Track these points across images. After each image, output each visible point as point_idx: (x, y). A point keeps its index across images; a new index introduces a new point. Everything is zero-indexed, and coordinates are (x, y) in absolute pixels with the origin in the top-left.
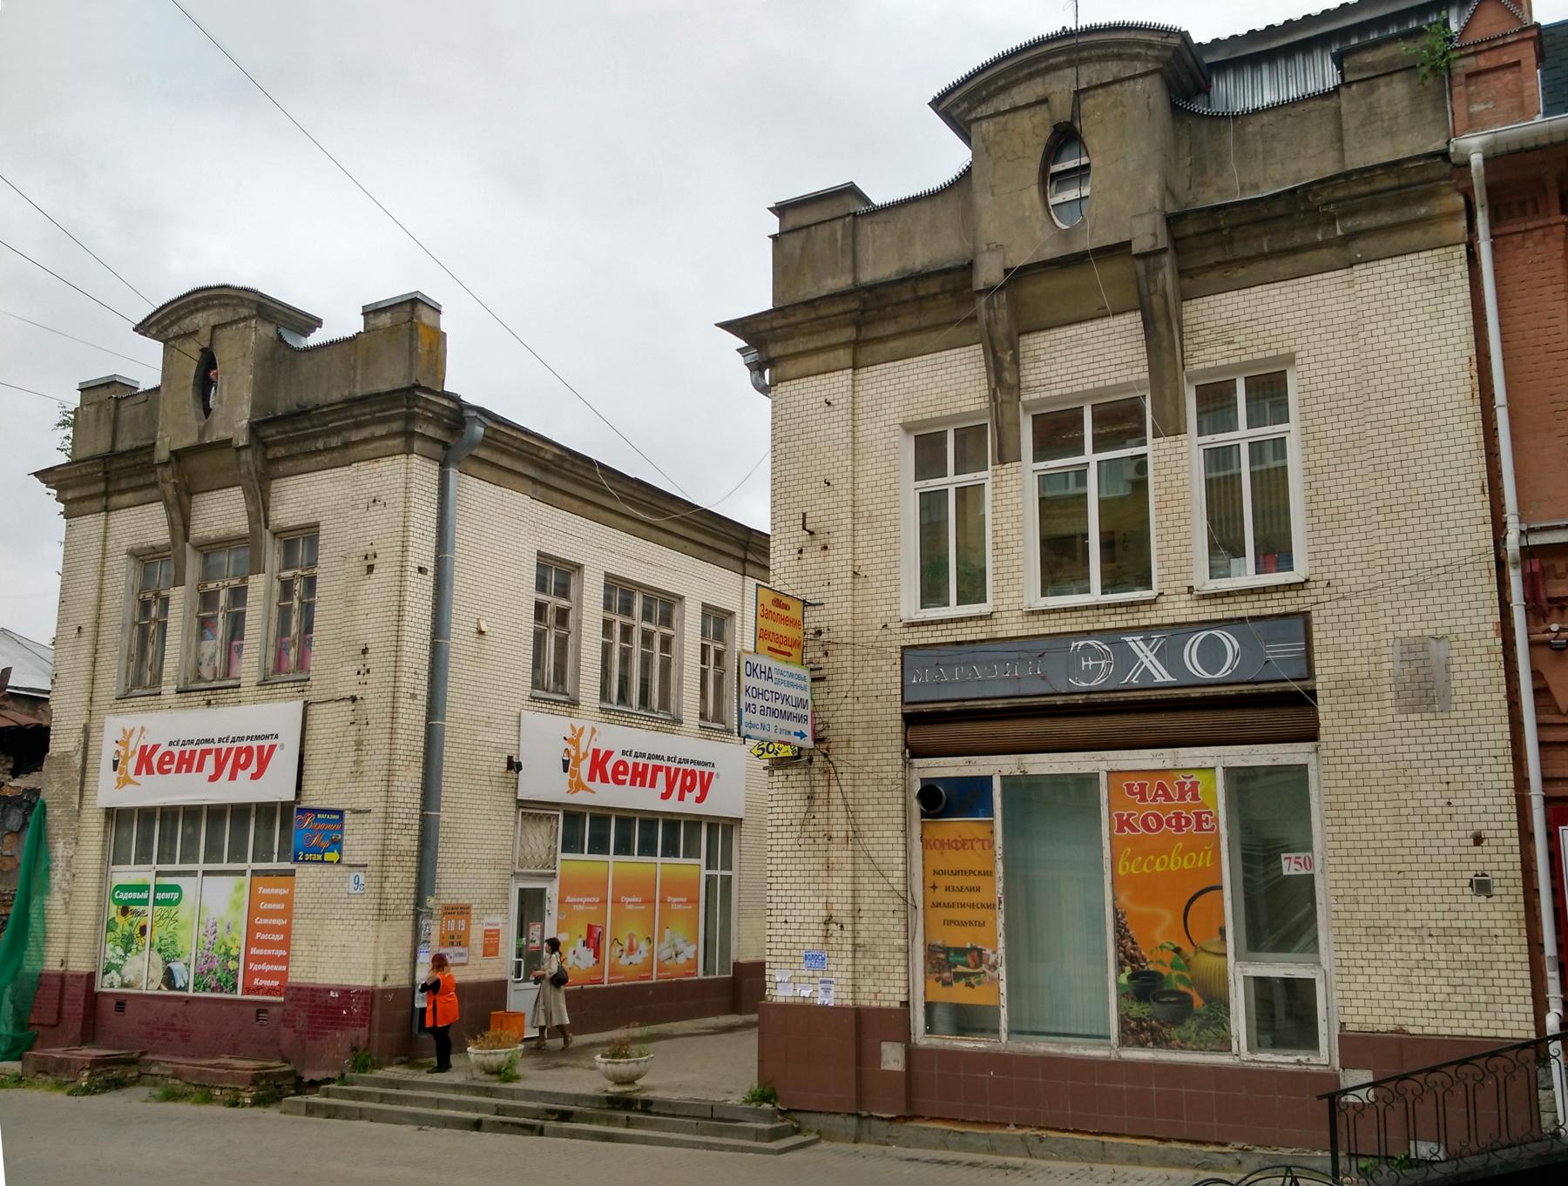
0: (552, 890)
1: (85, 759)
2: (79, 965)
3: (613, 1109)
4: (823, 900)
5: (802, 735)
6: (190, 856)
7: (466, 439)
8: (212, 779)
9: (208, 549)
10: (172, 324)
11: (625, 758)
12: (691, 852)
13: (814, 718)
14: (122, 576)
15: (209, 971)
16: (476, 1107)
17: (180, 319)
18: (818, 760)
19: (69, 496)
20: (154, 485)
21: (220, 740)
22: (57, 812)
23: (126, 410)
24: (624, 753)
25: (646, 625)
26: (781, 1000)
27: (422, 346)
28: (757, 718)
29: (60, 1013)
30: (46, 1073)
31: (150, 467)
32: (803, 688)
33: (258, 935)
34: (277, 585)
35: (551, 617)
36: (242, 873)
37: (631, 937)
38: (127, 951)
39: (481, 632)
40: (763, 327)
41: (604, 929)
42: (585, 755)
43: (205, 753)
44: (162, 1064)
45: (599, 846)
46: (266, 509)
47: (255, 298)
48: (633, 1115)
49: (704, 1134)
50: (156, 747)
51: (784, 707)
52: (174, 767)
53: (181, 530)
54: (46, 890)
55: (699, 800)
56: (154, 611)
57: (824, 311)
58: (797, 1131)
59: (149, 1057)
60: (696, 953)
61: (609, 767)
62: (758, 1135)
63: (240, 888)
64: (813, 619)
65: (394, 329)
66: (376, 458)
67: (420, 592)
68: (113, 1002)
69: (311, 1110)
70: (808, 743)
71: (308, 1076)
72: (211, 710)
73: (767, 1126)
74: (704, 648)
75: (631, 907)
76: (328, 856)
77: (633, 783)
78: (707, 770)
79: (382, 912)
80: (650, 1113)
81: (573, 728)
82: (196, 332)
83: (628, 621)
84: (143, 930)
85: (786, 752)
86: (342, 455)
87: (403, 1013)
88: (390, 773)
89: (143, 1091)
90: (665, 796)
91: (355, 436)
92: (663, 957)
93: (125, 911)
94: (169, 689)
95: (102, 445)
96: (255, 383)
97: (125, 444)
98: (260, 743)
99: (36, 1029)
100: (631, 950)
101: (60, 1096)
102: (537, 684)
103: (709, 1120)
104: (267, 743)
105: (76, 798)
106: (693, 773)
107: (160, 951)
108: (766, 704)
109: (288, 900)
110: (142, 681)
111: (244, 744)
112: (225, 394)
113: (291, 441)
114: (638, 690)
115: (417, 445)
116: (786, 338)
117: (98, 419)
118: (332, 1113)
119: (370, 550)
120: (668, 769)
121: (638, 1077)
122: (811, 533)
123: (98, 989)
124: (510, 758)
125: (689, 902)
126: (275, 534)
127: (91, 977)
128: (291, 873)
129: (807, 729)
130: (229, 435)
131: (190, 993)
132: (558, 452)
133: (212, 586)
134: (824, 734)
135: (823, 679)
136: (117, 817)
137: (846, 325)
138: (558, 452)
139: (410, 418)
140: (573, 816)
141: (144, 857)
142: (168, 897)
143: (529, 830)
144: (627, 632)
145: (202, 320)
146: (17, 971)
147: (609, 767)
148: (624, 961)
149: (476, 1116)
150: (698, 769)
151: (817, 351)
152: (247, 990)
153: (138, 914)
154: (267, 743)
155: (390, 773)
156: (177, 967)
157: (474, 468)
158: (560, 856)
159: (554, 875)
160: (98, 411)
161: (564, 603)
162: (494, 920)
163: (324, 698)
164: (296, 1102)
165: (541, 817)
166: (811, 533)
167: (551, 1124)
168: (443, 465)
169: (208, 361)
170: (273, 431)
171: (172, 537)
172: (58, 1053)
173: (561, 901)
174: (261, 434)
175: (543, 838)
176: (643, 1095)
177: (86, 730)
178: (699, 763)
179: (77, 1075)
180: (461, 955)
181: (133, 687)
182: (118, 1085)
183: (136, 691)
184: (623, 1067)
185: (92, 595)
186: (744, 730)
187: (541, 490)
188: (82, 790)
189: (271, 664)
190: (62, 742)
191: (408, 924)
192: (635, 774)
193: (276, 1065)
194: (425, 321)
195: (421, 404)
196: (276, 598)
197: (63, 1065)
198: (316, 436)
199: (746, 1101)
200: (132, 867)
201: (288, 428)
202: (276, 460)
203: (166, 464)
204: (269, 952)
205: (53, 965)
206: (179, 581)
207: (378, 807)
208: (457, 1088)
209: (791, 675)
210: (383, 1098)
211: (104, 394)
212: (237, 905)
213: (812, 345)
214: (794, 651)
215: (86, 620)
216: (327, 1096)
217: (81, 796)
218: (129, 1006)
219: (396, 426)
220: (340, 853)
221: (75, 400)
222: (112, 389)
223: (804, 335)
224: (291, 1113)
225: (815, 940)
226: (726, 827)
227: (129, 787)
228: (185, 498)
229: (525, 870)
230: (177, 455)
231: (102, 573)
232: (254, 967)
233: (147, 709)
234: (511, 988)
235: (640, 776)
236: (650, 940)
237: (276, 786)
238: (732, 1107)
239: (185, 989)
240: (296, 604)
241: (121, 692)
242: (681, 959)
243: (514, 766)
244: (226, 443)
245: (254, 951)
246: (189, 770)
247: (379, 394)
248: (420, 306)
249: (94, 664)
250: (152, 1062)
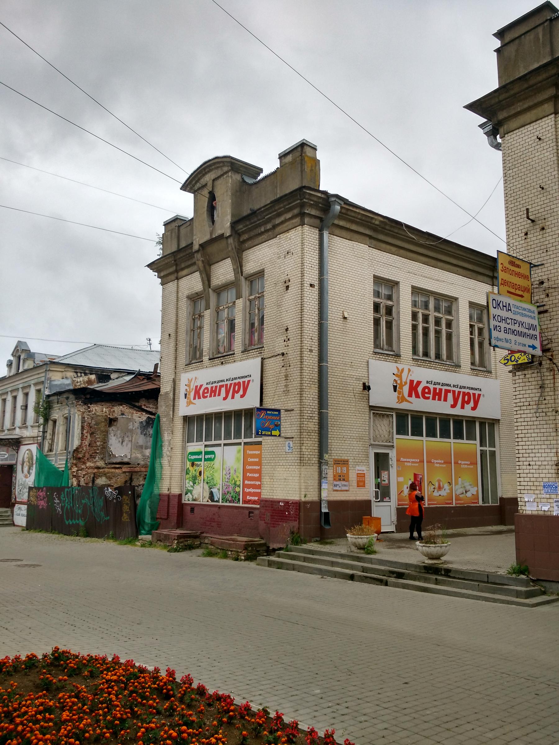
0: (393, 454)
1: (174, 394)
2: (176, 491)
3: (428, 573)
4: (554, 451)
5: (534, 347)
6: (218, 437)
7: (331, 214)
8: (225, 399)
9: (220, 290)
10: (196, 183)
11: (428, 385)
12: (471, 437)
13: (541, 337)
15: (228, 492)
16: (352, 567)
17: (199, 179)
18: (546, 363)
19: (162, 274)
20: (194, 264)
21: (227, 380)
22: (164, 420)
24: (428, 382)
25: (437, 314)
26: (529, 513)
27: (307, 168)
28: (502, 335)
29: (168, 513)
30: (160, 541)
31: (191, 255)
32: (534, 318)
33: (248, 474)
35: (383, 311)
36: (240, 444)
37: (439, 481)
38: (194, 483)
39: (345, 318)
40: (493, 102)
41: (423, 476)
42: (406, 383)
43: (221, 386)
44: (211, 537)
45: (417, 432)
46: (241, 266)
47: (228, 160)
48: (439, 578)
49: (482, 591)
50: (201, 386)
51: (521, 329)
52: (209, 394)
53: (206, 282)
54: (161, 456)
55: (474, 409)
57: (532, 82)
58: (544, 593)
59: (204, 535)
60: (477, 491)
61: (420, 389)
62: (518, 594)
63: (239, 451)
64: (537, 275)
65: (292, 163)
66: (287, 231)
67: (312, 296)
68: (189, 508)
69: (271, 564)
70: (538, 352)
71: (272, 546)
72: (223, 366)
73: (524, 589)
74: (471, 326)
75: (438, 465)
76: (274, 433)
77: (434, 399)
78: (477, 392)
79: (302, 461)
80: (450, 577)
81: (397, 368)
82: (206, 185)
83: (426, 312)
84: (200, 473)
85: (523, 359)
86: (273, 232)
87: (315, 514)
88: (302, 390)
89: (200, 551)
90: (453, 406)
91: (278, 221)
92: (458, 493)
93: (193, 465)
94: (206, 359)
95: (174, 248)
96: (233, 203)
97: (183, 244)
98: (243, 380)
99: (159, 520)
100: (440, 488)
101: (165, 552)
102: (377, 345)
103: (485, 583)
104: (246, 380)
105: (171, 413)
106: (468, 394)
107: (207, 483)
108: (508, 326)
109: (259, 456)
110: (195, 357)
111: (237, 381)
112: (220, 211)
113: (250, 230)
114: (434, 345)
115: (306, 220)
116: (509, 106)
117: (171, 236)
118: (280, 566)
120: (454, 392)
121: (442, 555)
122: (533, 221)
123: (183, 502)
124: (364, 384)
125: (471, 464)
126: (246, 279)
127: (180, 496)
128: (260, 443)
129: (537, 344)
131: (220, 504)
132: (382, 219)
134: (549, 346)
135: (546, 311)
136: (188, 420)
137: (549, 87)
138: (382, 219)
139: (302, 206)
140: (402, 416)
141: (199, 439)
142: (210, 456)
143: (377, 422)
144: (426, 319)
145: (208, 178)
146: (152, 493)
147: (420, 389)
148: (436, 494)
149: (350, 572)
150: (471, 392)
151: (529, 109)
152: (245, 502)
153: (198, 465)
154: (246, 380)
155: (302, 390)
156: (214, 490)
157: (337, 231)
158: (396, 436)
159: (393, 446)
160: (171, 233)
161: (390, 303)
162: (362, 468)
163: (270, 355)
164: (264, 560)
165: (383, 415)
166: (533, 221)
167: (392, 580)
168: (321, 230)
169: (212, 197)
170: (241, 227)
171: (203, 287)
172: (165, 532)
173: (398, 460)
174: (236, 229)
175: (387, 427)
176: (445, 566)
177: (174, 381)
178: (472, 389)
179: (173, 543)
180: (345, 485)
181: (192, 359)
182: (190, 548)
183: (193, 361)
184: (433, 549)
185: (174, 319)
186: (493, 342)
187: (374, 242)
188: (173, 409)
189: (247, 342)
190: (165, 388)
191: (316, 468)
192: (435, 394)
193: (257, 540)
194: (309, 154)
195: (307, 197)
197: (167, 537)
198: (260, 226)
199: (509, 573)
200: (195, 443)
201: (248, 223)
202: (244, 241)
203: (197, 251)
204: (253, 483)
205: (165, 491)
206: (207, 307)
207: (296, 407)
208: (342, 556)
209: (524, 309)
210: (305, 559)
212: (238, 460)
213: (526, 106)
214: (526, 295)
215: (172, 331)
216: (279, 557)
217: (173, 412)
218: (196, 510)
219: (296, 211)
220: (280, 431)
221: (162, 230)
222: (176, 222)
223: (519, 101)
224: (261, 565)
225: (550, 475)
226: (489, 425)
227: (191, 405)
228: (207, 267)
229: (376, 443)
230: (203, 246)
231: (177, 308)
232: (247, 490)
233: (197, 369)
234: (374, 505)
235: (438, 395)
236: (450, 483)
237: (251, 400)
238: (501, 576)
239: (218, 501)
241: (187, 362)
242: (469, 495)
243: (366, 388)
244: (221, 236)
245: (246, 482)
246: (215, 396)
247: (286, 195)
248: (305, 147)
249: (176, 350)
250: (205, 537)
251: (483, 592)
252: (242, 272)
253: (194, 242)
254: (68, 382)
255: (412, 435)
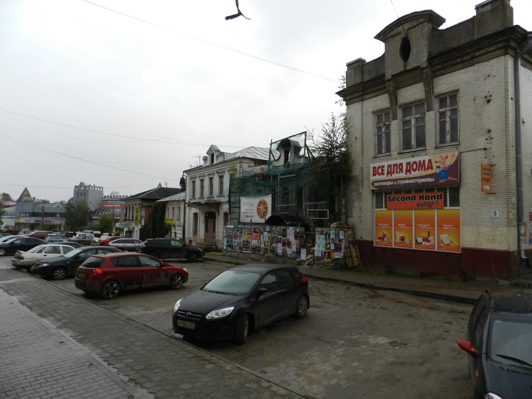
14: (370, 122)
19: (348, 98)
23: (365, 68)
31: (384, 82)
34: (438, 114)
56: (383, 130)
91: (477, 54)
117: (355, 73)
119: (487, 94)
126: (436, 97)
130: (418, 64)
133: (408, 118)
139: (508, 40)
145: (407, 26)
160: (355, 70)
196: (438, 119)
198: (456, 58)
202: (437, 71)
203: (390, 80)
206: (395, 118)
211: (357, 65)
240: (448, 119)
251: (121, 271)
252: (433, 93)
253: (386, 74)
254: (251, 169)
255: (450, 206)
